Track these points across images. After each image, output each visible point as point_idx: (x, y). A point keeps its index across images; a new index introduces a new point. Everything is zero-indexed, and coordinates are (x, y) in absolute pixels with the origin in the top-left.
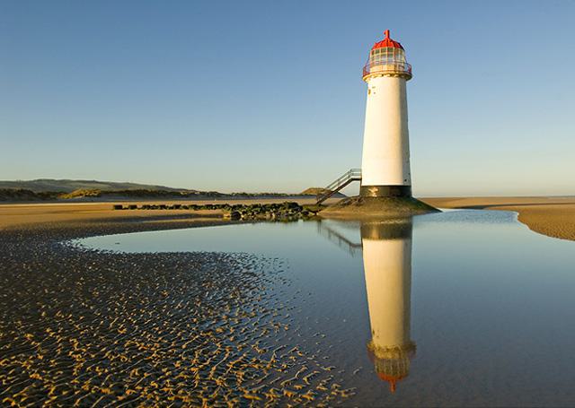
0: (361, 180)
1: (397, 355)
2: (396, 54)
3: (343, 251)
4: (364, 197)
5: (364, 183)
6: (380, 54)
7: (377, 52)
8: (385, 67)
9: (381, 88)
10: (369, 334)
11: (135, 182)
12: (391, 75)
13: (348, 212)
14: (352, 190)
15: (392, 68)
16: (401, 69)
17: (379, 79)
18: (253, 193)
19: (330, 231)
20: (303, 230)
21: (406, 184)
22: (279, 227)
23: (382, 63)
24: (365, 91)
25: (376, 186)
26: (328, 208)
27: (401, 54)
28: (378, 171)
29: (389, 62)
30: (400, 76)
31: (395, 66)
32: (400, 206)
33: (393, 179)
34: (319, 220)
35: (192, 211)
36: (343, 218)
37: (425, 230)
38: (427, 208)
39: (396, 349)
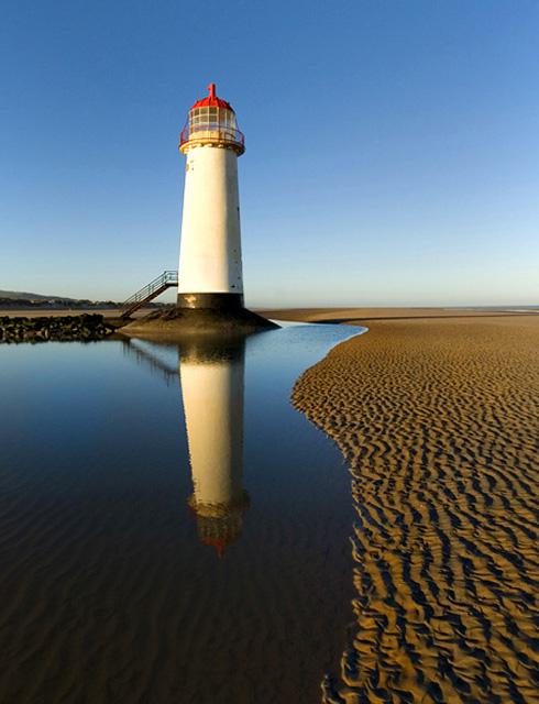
0: (176, 285)
1: (222, 512)
2: (222, 119)
3: (157, 378)
4: (176, 312)
5: (181, 290)
6: (200, 115)
7: (197, 113)
8: (207, 134)
9: (203, 163)
10: (189, 487)
11: (244, 265)
12: (214, 145)
13: (150, 329)
14: (169, 297)
15: (215, 135)
16: (229, 137)
17: (199, 149)
18: (122, 301)
19: (140, 352)
20: (106, 352)
21: (234, 291)
22: (26, 347)
23: (203, 128)
24: (181, 165)
25: (194, 294)
26: (133, 323)
27: (229, 118)
28: (199, 275)
29: (211, 128)
30: (225, 146)
31: (220, 135)
32: (228, 323)
33: (215, 284)
34: (126, 340)
35: (517, 486)
36: (146, 335)
37: (262, 353)
38: (261, 322)
39: (219, 506)
